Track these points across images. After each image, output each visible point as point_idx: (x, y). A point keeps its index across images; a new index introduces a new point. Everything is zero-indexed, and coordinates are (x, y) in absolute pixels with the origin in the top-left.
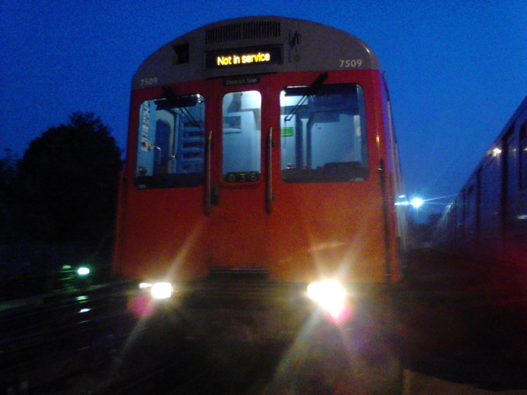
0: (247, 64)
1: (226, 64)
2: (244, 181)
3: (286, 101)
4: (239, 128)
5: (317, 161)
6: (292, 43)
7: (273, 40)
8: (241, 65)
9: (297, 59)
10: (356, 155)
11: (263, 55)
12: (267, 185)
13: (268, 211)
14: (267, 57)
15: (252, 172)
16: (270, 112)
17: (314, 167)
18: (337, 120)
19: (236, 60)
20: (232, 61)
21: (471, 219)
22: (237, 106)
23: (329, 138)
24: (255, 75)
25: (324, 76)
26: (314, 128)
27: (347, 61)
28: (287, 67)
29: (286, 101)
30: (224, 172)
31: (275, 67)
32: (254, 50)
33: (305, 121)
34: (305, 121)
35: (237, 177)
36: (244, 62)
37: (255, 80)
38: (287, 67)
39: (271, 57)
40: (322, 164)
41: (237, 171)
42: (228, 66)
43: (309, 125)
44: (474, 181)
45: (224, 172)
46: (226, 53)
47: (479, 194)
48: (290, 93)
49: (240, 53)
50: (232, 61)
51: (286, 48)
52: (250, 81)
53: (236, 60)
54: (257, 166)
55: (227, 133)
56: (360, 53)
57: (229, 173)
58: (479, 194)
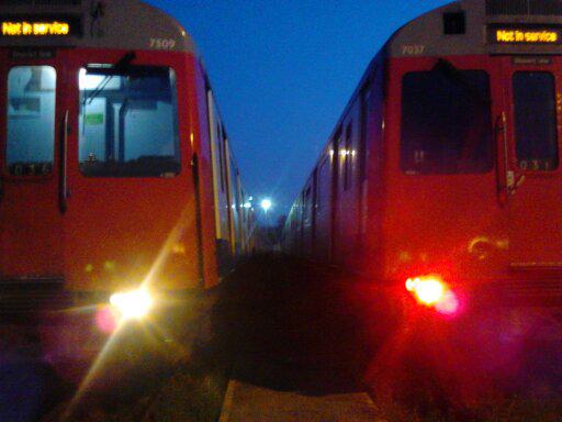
0: (39, 36)
1: (507, 40)
2: (31, 173)
3: (87, 81)
4: (39, 110)
5: (132, 151)
6: (95, 15)
7: (75, 10)
8: (32, 36)
9: (100, 33)
10: (168, 150)
11: (548, 34)
12: (61, 179)
13: (62, 210)
14: (63, 29)
15: (42, 164)
16: (68, 96)
17: (128, 157)
18: (154, 107)
19: (27, 28)
20: (21, 29)
21: (308, 223)
22: (35, 83)
23: (143, 128)
24: (547, 55)
25: (131, 55)
26: (129, 116)
27: (158, 41)
28: (88, 42)
29: (87, 81)
30: (9, 161)
31: (76, 41)
32: (48, 19)
33: (117, 107)
34: (117, 107)
35: (26, 168)
36: (528, 39)
37: (49, 54)
38: (88, 42)
39: (70, 28)
40: (136, 157)
41: (25, 160)
42: (16, 36)
43: (122, 112)
44: (311, 183)
45: (9, 161)
46: (15, 19)
47: (315, 195)
48: (91, 71)
49: (32, 20)
50: (21, 29)
51: (88, 19)
52: (42, 54)
53: (27, 28)
54: (49, 156)
55: (14, 117)
56: (176, 35)
57: (14, 165)
58: (315, 195)
